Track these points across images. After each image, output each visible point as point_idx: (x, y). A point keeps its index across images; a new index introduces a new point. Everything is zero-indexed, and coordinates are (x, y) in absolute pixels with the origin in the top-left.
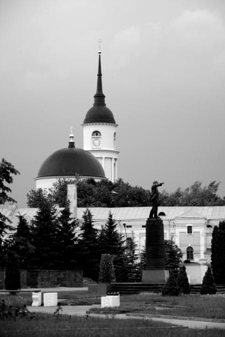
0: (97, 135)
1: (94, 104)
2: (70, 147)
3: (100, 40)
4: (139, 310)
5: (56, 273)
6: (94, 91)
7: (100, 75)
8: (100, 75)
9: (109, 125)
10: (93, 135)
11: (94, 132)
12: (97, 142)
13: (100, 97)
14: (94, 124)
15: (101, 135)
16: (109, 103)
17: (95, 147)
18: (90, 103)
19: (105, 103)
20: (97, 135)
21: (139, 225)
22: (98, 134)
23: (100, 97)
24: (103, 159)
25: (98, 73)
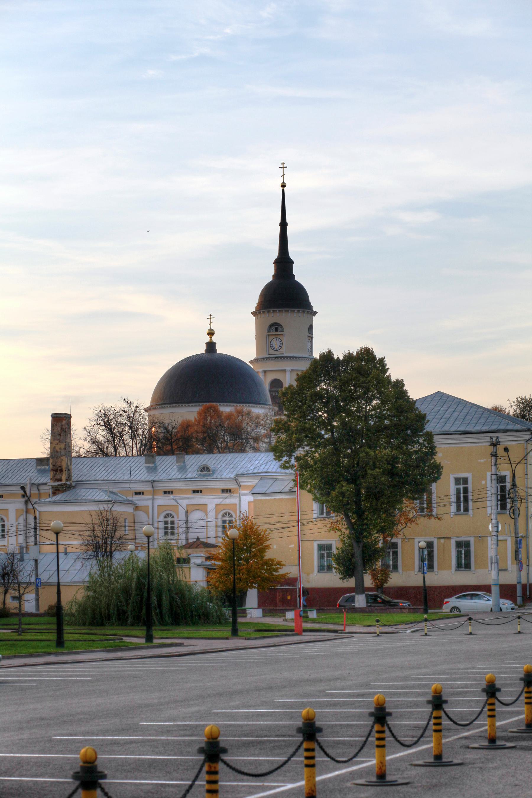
0: (276, 330)
1: (274, 276)
2: (207, 351)
3: (283, 164)
4: (220, 695)
5: (231, 615)
6: (275, 252)
7: (284, 224)
8: (284, 224)
9: (304, 312)
10: (269, 331)
11: (271, 326)
12: (276, 344)
13: (284, 263)
14: (277, 310)
15: (283, 331)
16: (300, 274)
17: (272, 352)
18: (267, 274)
19: (294, 273)
20: (276, 330)
21: (188, 489)
22: (279, 328)
23: (284, 263)
24: (288, 374)
25: (280, 221)
